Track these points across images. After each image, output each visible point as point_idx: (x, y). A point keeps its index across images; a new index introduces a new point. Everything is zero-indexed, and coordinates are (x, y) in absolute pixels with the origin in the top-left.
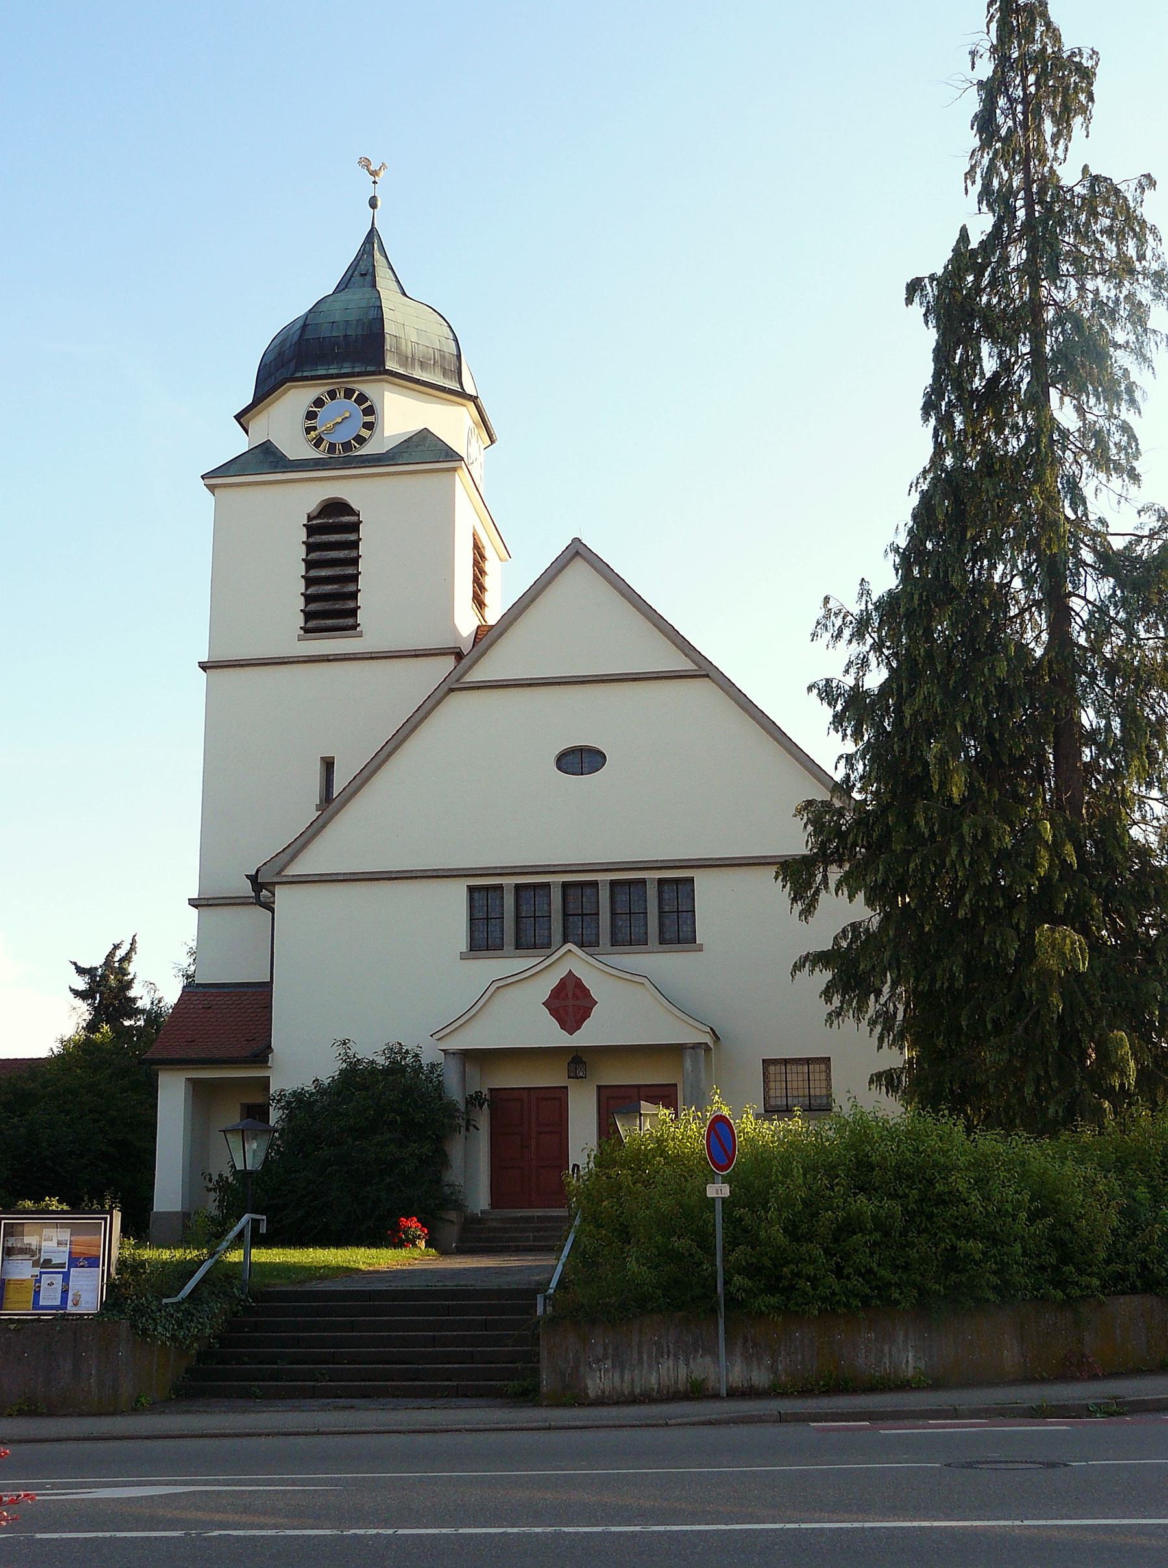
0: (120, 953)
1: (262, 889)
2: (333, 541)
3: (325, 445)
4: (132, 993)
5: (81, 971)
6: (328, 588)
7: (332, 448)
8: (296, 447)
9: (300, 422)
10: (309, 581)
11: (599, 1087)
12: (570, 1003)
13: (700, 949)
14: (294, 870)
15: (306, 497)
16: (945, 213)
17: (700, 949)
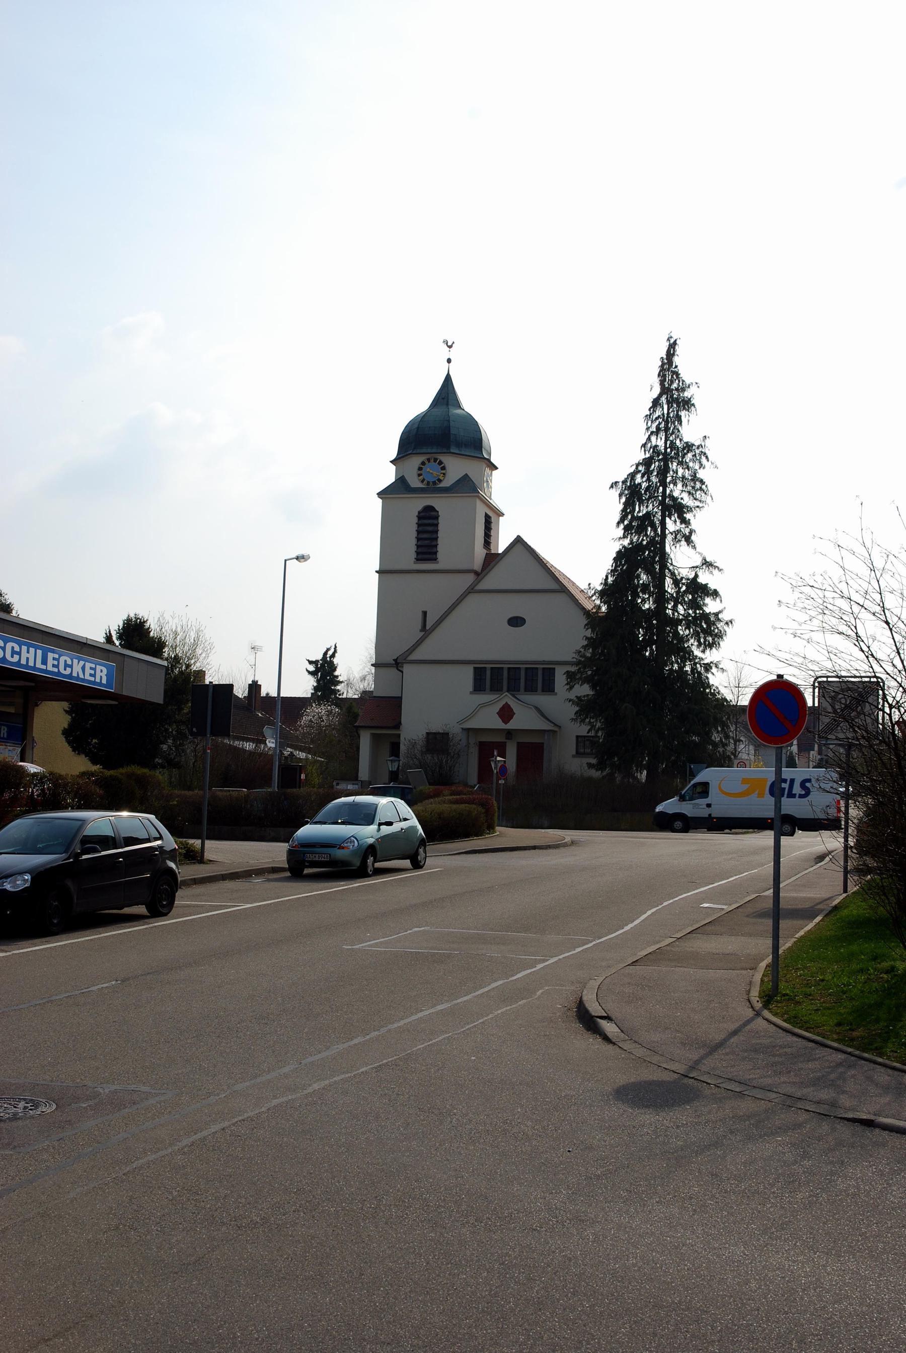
0: (330, 653)
1: (397, 664)
2: (428, 521)
3: (425, 482)
4: (336, 673)
5: (310, 662)
6: (426, 542)
7: (428, 483)
8: (415, 483)
9: (415, 471)
10: (418, 539)
11: (518, 743)
12: (506, 713)
13: (556, 694)
14: (412, 657)
15: (418, 504)
16: (627, 453)
17: (556, 694)
